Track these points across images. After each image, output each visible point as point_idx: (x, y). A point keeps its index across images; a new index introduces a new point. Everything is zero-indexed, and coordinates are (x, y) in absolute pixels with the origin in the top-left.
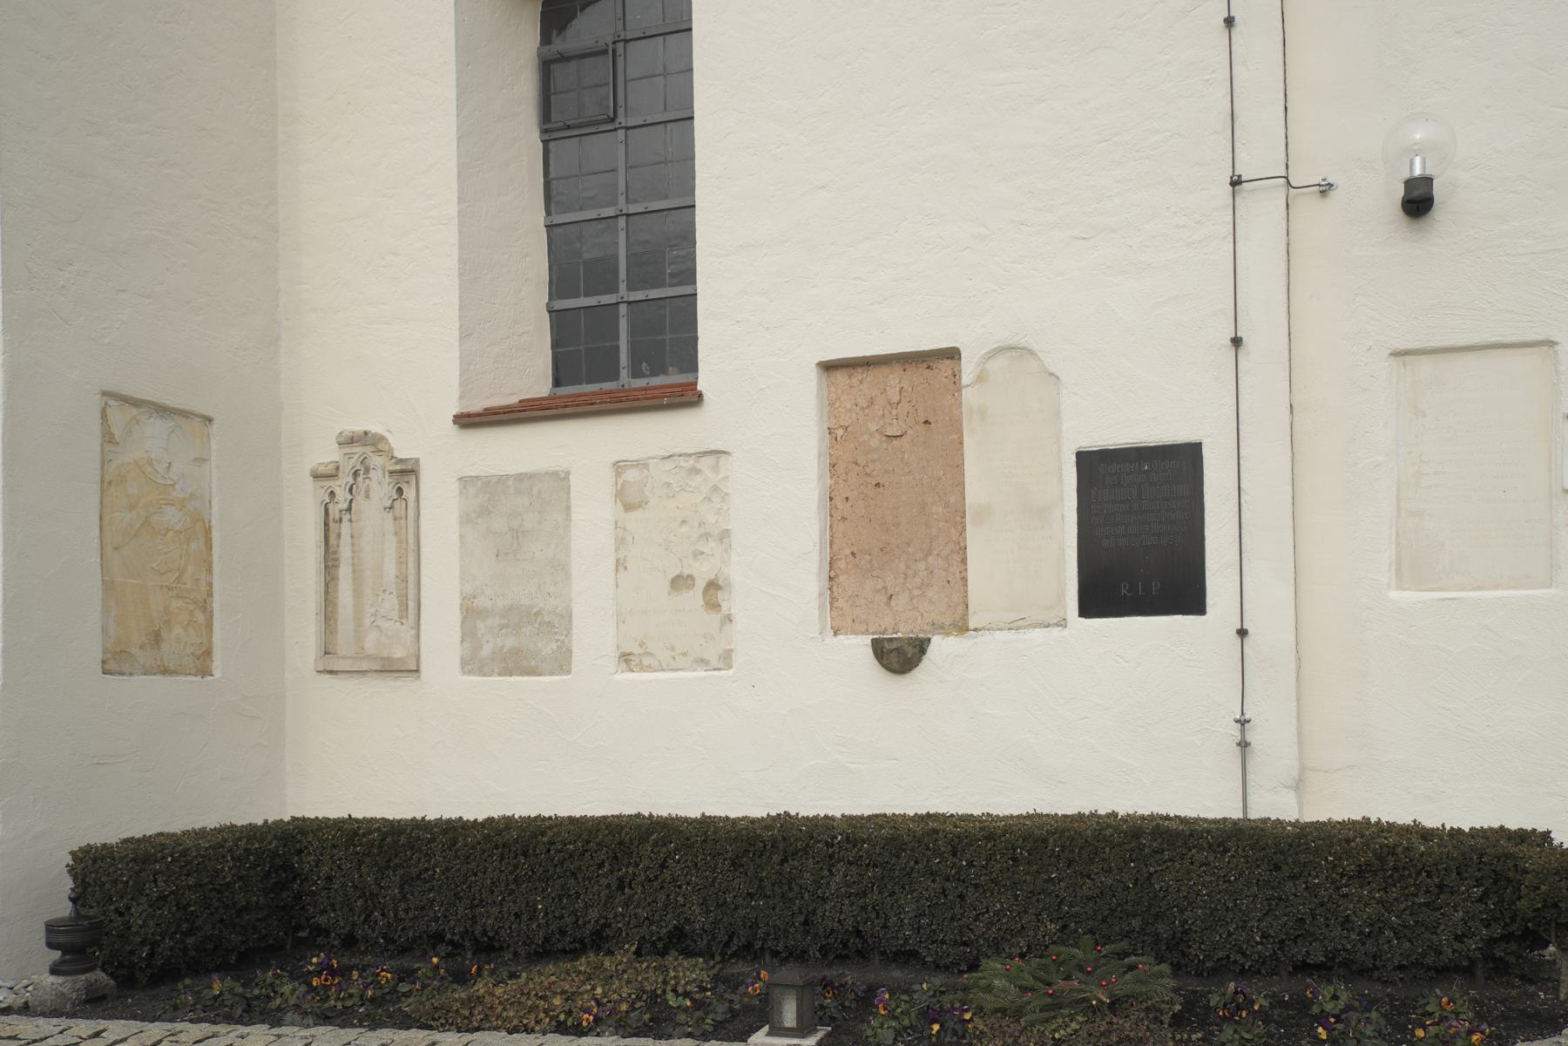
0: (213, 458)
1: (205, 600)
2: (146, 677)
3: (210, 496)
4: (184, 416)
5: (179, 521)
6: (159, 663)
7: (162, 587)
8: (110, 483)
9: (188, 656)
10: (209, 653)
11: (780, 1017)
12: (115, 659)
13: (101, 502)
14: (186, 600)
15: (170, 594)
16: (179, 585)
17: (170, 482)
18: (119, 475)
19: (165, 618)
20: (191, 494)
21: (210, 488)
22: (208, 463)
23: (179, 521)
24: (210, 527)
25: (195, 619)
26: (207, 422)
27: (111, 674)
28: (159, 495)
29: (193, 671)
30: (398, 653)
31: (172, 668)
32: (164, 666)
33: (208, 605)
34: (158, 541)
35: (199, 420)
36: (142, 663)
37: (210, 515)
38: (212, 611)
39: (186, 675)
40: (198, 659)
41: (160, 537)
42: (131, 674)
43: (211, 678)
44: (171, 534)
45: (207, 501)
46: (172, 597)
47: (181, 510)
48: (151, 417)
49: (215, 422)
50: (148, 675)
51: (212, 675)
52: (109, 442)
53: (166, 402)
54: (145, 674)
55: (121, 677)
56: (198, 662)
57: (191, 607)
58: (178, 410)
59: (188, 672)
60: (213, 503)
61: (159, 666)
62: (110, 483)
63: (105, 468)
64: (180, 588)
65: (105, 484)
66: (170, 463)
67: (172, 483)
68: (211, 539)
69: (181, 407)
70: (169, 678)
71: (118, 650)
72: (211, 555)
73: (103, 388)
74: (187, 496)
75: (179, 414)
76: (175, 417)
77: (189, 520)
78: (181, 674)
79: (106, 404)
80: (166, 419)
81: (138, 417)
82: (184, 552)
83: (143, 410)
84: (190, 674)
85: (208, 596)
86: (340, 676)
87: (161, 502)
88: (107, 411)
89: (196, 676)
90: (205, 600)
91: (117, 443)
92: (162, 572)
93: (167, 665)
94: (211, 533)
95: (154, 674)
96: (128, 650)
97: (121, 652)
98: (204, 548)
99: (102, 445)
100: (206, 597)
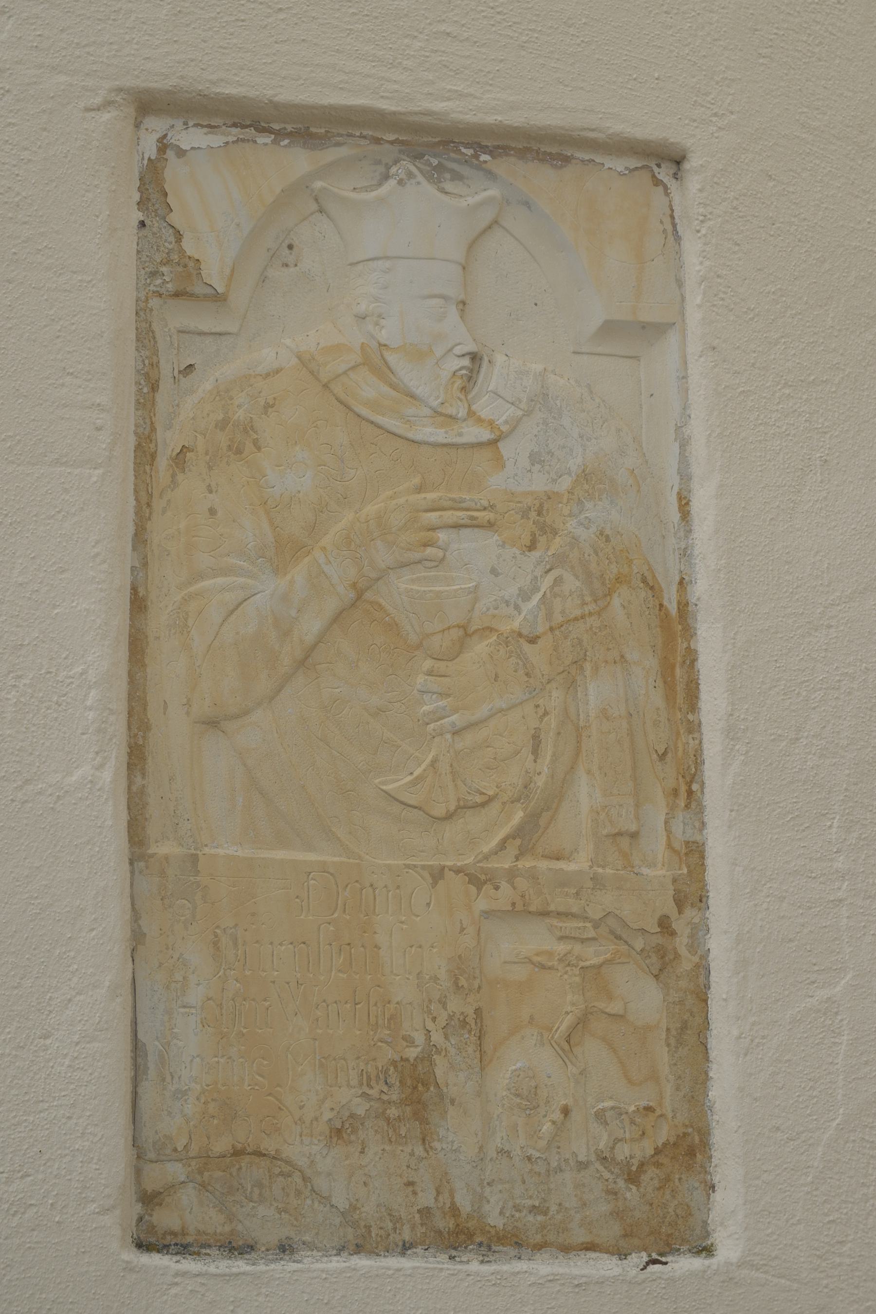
0: (694, 317)
1: (664, 924)
2: (362, 1262)
3: (685, 477)
4: (544, 158)
5: (525, 595)
6: (426, 1199)
7: (437, 875)
8: (180, 459)
9: (582, 1166)
10: (691, 1153)
11: (653, 142)
12: (203, 1186)
13: (140, 538)
14: (570, 925)
15: (482, 904)
16: (526, 863)
17: (474, 433)
18: (222, 425)
19: (455, 1005)
20: (585, 476)
21: (684, 444)
22: (673, 338)
23: (525, 595)
24: (684, 606)
25: (615, 1007)
26: (664, 174)
27: (184, 1249)
28: (420, 489)
29: (611, 1232)
30: (454, 414)
31: (495, 1220)
32: (454, 1211)
33: (681, 942)
34: (421, 679)
35: (619, 164)
36: (341, 1201)
37: (686, 554)
38: (703, 968)
39: (566, 1249)
40: (633, 1178)
41: (428, 664)
42: (285, 1249)
43: (697, 1263)
44: (481, 648)
45: (673, 499)
46: (487, 914)
47: (532, 547)
48: (386, 177)
49: (693, 163)
50: (373, 1253)
51: (707, 1251)
52: (177, 295)
53: (440, 106)
54: (359, 1249)
55: (241, 1265)
56: (632, 1194)
57: (592, 955)
58: (514, 132)
59: (580, 1236)
60: (696, 506)
61: (425, 1212)
62: (180, 459)
63: (162, 399)
64: (533, 876)
65: (163, 462)
66: (475, 357)
67: (486, 435)
68: (691, 658)
69: (516, 119)
70: (475, 1266)
71: (221, 1146)
72: (694, 728)
73: (129, 82)
74: (565, 483)
75: (523, 153)
76: (502, 166)
77: (571, 583)
78: (539, 1247)
79: (163, 146)
80: (457, 177)
81: (318, 184)
82: (552, 721)
83: (343, 152)
84: (590, 1247)
85: (680, 903)
86: (128, 875)
87: (433, 517)
88: (168, 174)
89: (623, 1255)
90: (664, 924)
91: (218, 298)
92: (439, 810)
93: (464, 1203)
94: (689, 632)
95: (405, 1248)
96: (269, 1145)
97: (237, 1153)
98: (657, 699)
99: (142, 311)
100: (670, 908)
